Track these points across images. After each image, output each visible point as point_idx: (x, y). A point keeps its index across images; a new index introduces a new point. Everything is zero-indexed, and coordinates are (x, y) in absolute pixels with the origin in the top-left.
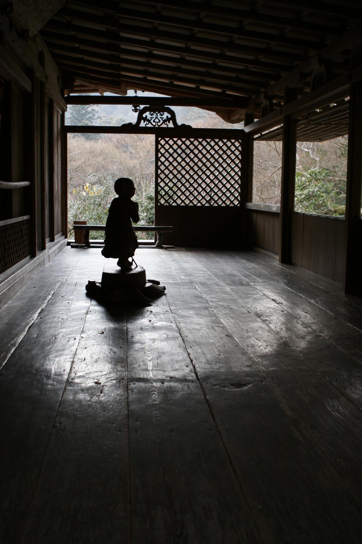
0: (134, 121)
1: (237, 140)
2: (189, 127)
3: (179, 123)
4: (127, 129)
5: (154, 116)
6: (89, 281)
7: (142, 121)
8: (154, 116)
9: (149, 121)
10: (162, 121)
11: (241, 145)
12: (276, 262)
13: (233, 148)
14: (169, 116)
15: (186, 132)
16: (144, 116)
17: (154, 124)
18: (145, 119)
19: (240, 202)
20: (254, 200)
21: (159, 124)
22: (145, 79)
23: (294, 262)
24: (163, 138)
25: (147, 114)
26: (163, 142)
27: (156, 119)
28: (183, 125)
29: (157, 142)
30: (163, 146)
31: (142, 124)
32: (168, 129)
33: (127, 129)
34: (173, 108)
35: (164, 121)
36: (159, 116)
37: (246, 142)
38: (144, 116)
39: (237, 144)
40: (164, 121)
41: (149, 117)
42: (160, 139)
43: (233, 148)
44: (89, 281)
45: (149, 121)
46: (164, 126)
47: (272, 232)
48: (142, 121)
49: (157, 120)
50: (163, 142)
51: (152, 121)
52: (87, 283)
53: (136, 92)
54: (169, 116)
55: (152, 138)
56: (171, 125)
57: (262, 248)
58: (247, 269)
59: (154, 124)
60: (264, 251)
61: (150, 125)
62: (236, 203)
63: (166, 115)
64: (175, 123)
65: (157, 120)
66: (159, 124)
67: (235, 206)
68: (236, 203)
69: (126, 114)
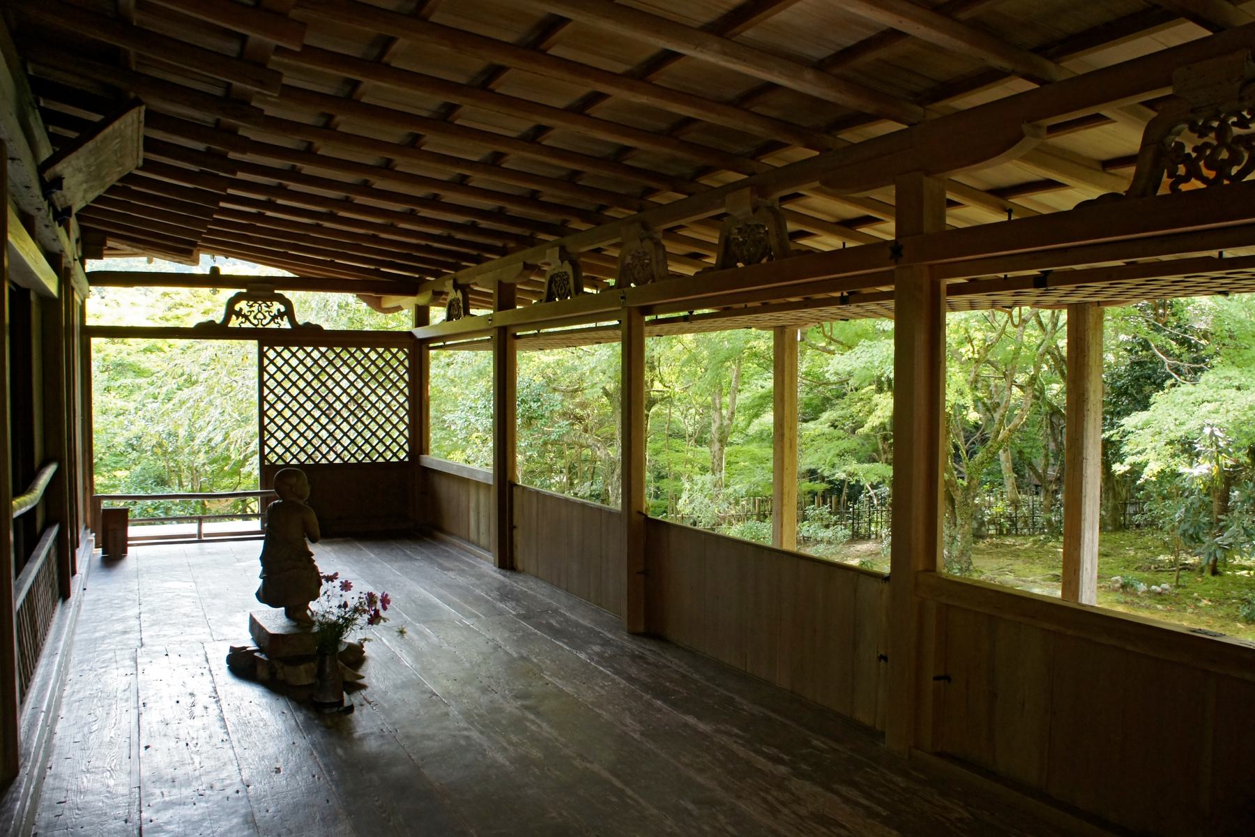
0: (218, 318)
1: (400, 349)
2: (318, 328)
3: (300, 320)
4: (207, 331)
5: (255, 309)
6: (232, 649)
7: (234, 317)
8: (255, 309)
9: (246, 317)
10: (269, 318)
11: (408, 356)
12: (487, 565)
13: (395, 363)
14: (283, 309)
15: (309, 335)
16: (237, 308)
17: (255, 322)
18: (239, 314)
19: (408, 454)
20: (431, 453)
21: (265, 322)
22: (474, 224)
23: (520, 566)
24: (271, 347)
25: (242, 305)
26: (271, 354)
27: (262, 314)
28: (308, 325)
29: (262, 355)
30: (272, 362)
31: (234, 323)
32: (280, 331)
33: (207, 331)
34: (288, 294)
35: (274, 318)
36: (264, 309)
37: (417, 351)
38: (237, 308)
39: (401, 356)
40: (274, 318)
41: (246, 310)
42: (266, 348)
43: (395, 363)
44: (232, 649)
45: (246, 317)
46: (273, 326)
47: (479, 516)
48: (234, 317)
49: (260, 316)
50: (271, 354)
51: (251, 318)
52: (227, 653)
53: (150, 261)
54: (283, 309)
55: (252, 346)
56: (285, 324)
57: (450, 534)
58: (448, 586)
59: (255, 322)
60: (457, 541)
61: (247, 325)
62: (402, 455)
63: (277, 306)
64: (292, 319)
65: (260, 316)
66: (265, 322)
67: (401, 461)
68: (402, 455)
69: (209, 305)
